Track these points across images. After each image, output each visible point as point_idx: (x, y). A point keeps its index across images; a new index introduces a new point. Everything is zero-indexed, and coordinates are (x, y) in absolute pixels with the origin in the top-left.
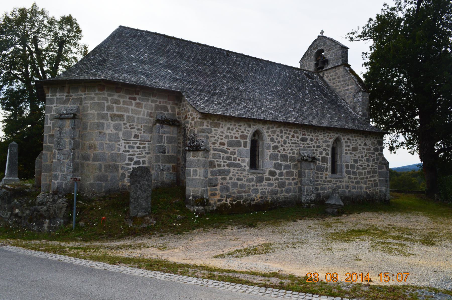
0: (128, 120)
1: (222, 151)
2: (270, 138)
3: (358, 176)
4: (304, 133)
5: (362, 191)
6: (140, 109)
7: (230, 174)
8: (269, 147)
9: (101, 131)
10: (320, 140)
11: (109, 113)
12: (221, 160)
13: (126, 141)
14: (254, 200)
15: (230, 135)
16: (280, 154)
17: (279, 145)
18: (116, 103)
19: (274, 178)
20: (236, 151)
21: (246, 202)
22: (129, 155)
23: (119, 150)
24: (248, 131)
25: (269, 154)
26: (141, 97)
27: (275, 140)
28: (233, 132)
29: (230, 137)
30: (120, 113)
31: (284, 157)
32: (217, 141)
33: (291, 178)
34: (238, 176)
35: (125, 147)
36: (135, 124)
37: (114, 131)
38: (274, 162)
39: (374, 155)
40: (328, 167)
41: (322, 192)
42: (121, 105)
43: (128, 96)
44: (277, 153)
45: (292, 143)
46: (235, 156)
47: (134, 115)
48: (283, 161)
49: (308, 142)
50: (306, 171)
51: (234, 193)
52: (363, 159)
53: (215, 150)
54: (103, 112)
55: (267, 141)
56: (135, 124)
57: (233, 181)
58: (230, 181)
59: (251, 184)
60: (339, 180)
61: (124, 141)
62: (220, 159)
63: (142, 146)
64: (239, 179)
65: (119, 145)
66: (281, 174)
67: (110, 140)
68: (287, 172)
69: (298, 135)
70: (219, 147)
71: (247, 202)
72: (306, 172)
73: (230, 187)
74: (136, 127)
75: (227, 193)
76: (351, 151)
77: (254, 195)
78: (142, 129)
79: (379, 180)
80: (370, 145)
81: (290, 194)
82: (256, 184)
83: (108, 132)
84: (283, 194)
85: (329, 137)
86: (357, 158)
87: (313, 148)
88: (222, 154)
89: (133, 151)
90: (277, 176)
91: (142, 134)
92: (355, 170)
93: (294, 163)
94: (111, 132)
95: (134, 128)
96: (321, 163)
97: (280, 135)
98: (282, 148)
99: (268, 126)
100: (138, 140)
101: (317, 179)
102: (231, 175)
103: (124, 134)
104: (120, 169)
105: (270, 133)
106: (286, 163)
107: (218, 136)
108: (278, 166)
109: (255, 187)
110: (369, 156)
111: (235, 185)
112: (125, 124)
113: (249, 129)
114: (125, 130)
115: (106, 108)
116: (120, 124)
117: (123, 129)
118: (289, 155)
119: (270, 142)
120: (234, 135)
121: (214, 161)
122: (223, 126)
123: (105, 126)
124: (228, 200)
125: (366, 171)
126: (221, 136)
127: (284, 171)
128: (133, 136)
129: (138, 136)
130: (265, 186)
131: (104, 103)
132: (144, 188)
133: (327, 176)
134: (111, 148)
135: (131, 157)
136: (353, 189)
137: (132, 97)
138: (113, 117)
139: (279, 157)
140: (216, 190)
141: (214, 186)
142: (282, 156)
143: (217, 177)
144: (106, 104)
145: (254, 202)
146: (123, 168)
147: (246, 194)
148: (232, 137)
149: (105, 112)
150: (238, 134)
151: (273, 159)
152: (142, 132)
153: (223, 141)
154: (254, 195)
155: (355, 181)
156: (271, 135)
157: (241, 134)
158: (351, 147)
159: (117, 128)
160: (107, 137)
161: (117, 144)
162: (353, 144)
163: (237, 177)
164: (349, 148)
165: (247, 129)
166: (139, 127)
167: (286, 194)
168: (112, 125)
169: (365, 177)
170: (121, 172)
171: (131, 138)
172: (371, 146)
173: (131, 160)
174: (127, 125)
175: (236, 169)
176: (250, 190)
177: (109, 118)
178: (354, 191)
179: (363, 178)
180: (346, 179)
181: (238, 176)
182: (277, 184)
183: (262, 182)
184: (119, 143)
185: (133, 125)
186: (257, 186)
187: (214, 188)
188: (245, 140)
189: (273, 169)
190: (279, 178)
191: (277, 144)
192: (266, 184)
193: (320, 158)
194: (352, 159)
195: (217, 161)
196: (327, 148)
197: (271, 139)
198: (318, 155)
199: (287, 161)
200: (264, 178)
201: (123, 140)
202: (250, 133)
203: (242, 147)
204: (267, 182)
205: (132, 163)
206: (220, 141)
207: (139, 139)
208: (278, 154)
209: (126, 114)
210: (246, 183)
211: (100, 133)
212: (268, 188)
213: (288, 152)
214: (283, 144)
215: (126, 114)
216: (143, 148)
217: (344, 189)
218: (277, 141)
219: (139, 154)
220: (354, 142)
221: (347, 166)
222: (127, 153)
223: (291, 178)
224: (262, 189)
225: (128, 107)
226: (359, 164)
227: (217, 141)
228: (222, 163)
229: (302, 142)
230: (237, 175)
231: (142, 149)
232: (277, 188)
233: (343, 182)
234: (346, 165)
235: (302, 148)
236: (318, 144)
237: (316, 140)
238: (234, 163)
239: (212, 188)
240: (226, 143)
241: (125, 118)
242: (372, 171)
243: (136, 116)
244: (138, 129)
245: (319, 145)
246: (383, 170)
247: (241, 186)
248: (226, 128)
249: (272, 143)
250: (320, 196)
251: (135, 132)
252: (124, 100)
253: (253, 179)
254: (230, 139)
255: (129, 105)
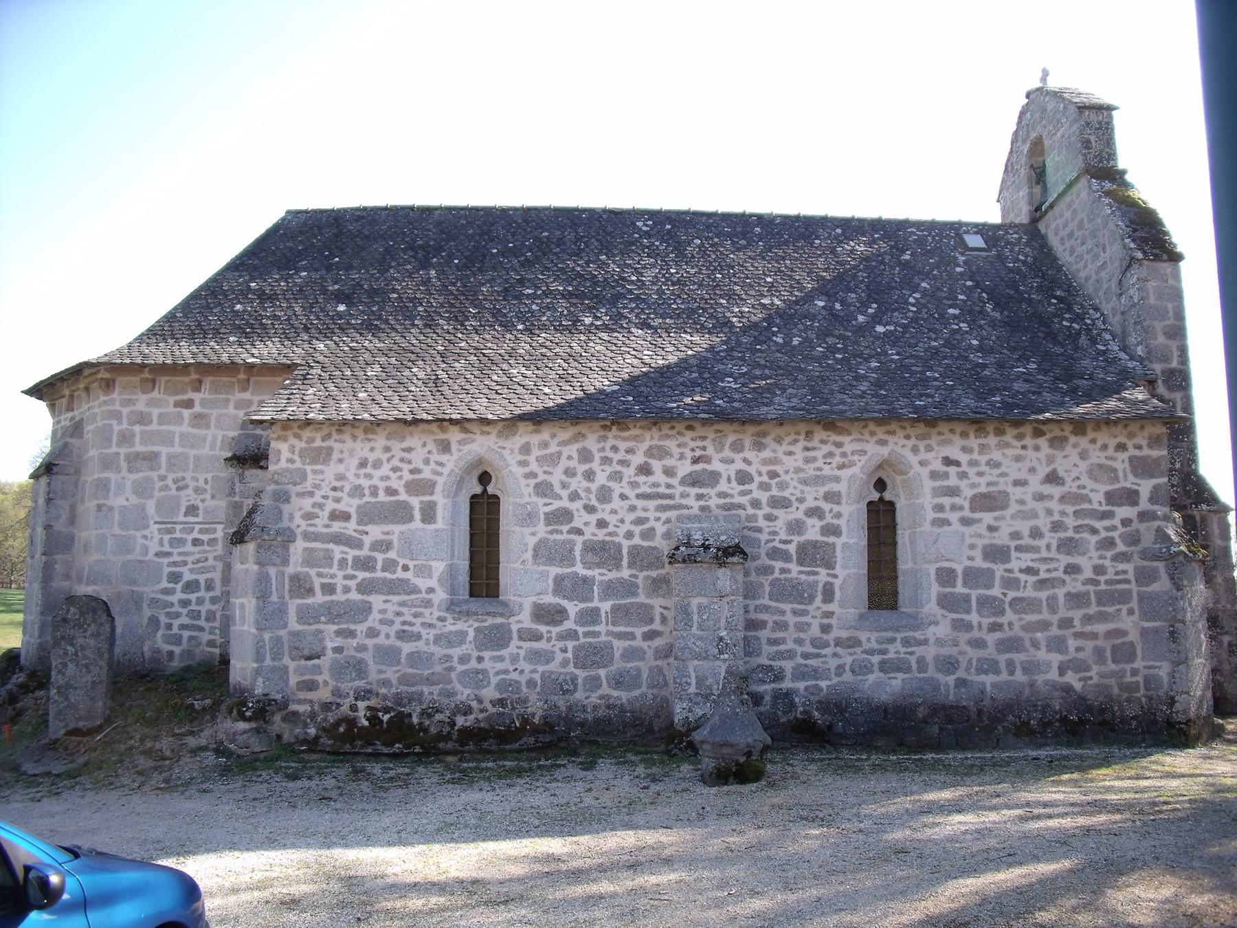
0: (172, 466)
1: (339, 539)
2: (532, 482)
3: (1010, 616)
4: (698, 453)
5: (1040, 678)
6: (202, 432)
7: (371, 618)
8: (529, 518)
9: (101, 502)
10: (786, 478)
11: (123, 451)
12: (334, 570)
13: (163, 526)
14: (467, 711)
15: (365, 483)
16: (579, 540)
17: (576, 506)
18: (139, 422)
19: (556, 630)
20: (395, 538)
21: (430, 716)
22: (169, 565)
23: (146, 550)
24: (441, 464)
25: (532, 541)
26: (207, 396)
27: (558, 489)
28: (377, 474)
29: (367, 491)
30: (150, 448)
31: (603, 553)
32: (321, 506)
33: (639, 631)
34: (404, 623)
35: (161, 544)
36: (188, 475)
37: (134, 500)
38: (554, 571)
39: (1106, 523)
40: (837, 583)
41: (801, 685)
42: (154, 426)
43: (172, 400)
44: (565, 536)
45: (638, 496)
46: (392, 555)
47: (186, 450)
48: (599, 566)
49: (723, 486)
50: (695, 602)
51: (386, 683)
52: (1042, 543)
53: (307, 536)
54: (109, 451)
55: (521, 496)
56: (188, 475)
57: (381, 640)
58: (370, 642)
59: (456, 652)
60: (899, 636)
61: (158, 526)
62: (331, 566)
63: (205, 537)
64: (402, 635)
65: (145, 537)
66: (590, 616)
67: (124, 526)
68: (615, 609)
69: (669, 462)
70: (327, 526)
71: (438, 717)
72: (695, 609)
73: (371, 663)
74: (192, 484)
75: (360, 684)
76: (967, 513)
77: (467, 692)
78: (208, 487)
79: (1144, 632)
80: (1085, 480)
81: (637, 693)
82: (475, 654)
83: (117, 502)
84: (600, 692)
85: (837, 460)
86: (1002, 538)
87: (750, 511)
88: (337, 551)
89: (180, 554)
90: (569, 625)
91: (207, 503)
92: (996, 591)
93: (654, 574)
94: (125, 503)
95: (186, 487)
96: (794, 568)
97: (581, 468)
98: (593, 519)
99: (525, 439)
100: (197, 520)
101: (780, 635)
102: (373, 620)
103: (159, 507)
104: (145, 605)
105: (534, 466)
106: (613, 575)
107: (325, 490)
108: (578, 588)
109: (473, 664)
110: (1077, 529)
111: (388, 655)
112: (163, 478)
113: (444, 458)
114: (163, 493)
115: (115, 440)
116: (149, 479)
117: (157, 494)
118: (626, 544)
119: (535, 499)
120: (382, 485)
121: (307, 575)
122: (346, 454)
123: (112, 487)
124: (361, 705)
125: (1060, 592)
126: (334, 489)
127: (606, 606)
128: (183, 510)
129: (197, 508)
130: (515, 659)
131: (110, 425)
132: (85, 657)
133: (833, 621)
134: (125, 546)
135: (178, 569)
136: (980, 671)
137: (182, 401)
138: (135, 460)
139: (577, 553)
140: (318, 670)
141: (309, 658)
142: (589, 548)
143: (321, 627)
144: (116, 428)
145: (471, 717)
146: (154, 601)
147: (436, 689)
148: (374, 491)
149: (114, 449)
150: (400, 478)
151: (550, 561)
152: (208, 496)
153: (342, 507)
154: (467, 692)
155: (991, 638)
156: (539, 471)
157: (411, 477)
158: (968, 493)
159: (142, 490)
160: (117, 517)
161: (139, 534)
162: (977, 479)
163: (397, 626)
164: (956, 500)
165: (435, 457)
166: (201, 483)
167: (615, 693)
168: (128, 484)
169: (1055, 619)
170: (147, 612)
171: (177, 515)
172: (1090, 484)
173: (175, 577)
174: (169, 481)
175: (395, 599)
176: (453, 675)
177: (124, 465)
178: (988, 680)
179: (1044, 625)
180: (943, 630)
181: (404, 623)
182: (570, 655)
183: (506, 646)
184: (146, 532)
185: (184, 478)
186: (480, 659)
187: (312, 662)
188: (427, 498)
189: (549, 599)
190: (581, 630)
191: (565, 503)
192: (522, 653)
193: (792, 548)
194: (972, 547)
195: (320, 575)
196: (826, 507)
197: (537, 486)
198: (783, 536)
199: (618, 567)
200: (510, 631)
201: (156, 523)
202: (446, 471)
203: (417, 524)
204: (527, 645)
205: (179, 587)
206: (330, 506)
207: (200, 519)
208: (572, 544)
209: (164, 451)
210: (433, 648)
211: (99, 507)
212: (527, 667)
213: (622, 531)
214: (594, 502)
215: (164, 451)
216: (209, 544)
217: (931, 672)
218: (565, 494)
219: (198, 561)
220: (980, 474)
221: (946, 577)
222: (166, 560)
223: (639, 631)
224: (506, 672)
225: (172, 428)
226: (1015, 564)
227: (321, 506)
228: (340, 582)
229: (694, 491)
230: (398, 620)
231: (206, 547)
232: (571, 668)
233: (925, 642)
234: (939, 571)
235: (695, 511)
236: (774, 492)
237: (765, 478)
238: (385, 579)
239: (303, 662)
240: (353, 511)
241: (163, 460)
242: (1098, 594)
243: (194, 452)
244: (197, 490)
245: (786, 494)
246: (1154, 587)
247: (414, 658)
248: (355, 462)
249: (541, 501)
250: (792, 705)
251: (188, 497)
252: (162, 410)
253: (463, 634)
254: (367, 499)
255: (175, 424)
